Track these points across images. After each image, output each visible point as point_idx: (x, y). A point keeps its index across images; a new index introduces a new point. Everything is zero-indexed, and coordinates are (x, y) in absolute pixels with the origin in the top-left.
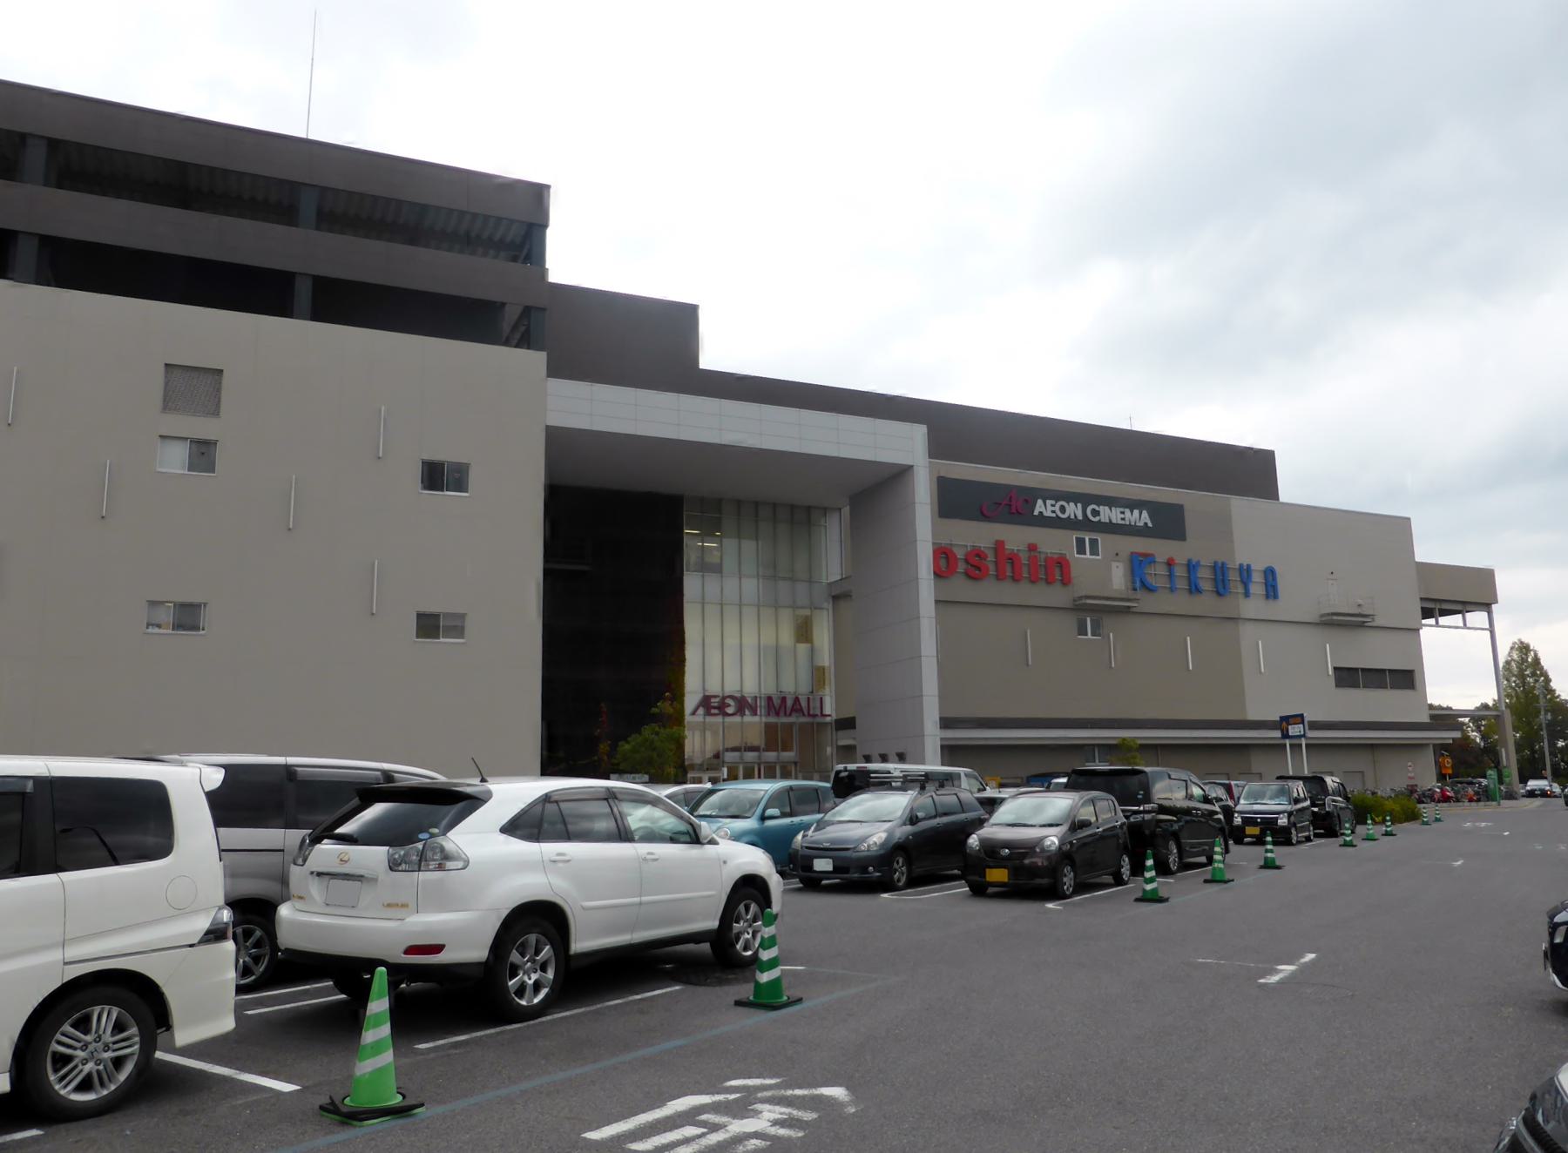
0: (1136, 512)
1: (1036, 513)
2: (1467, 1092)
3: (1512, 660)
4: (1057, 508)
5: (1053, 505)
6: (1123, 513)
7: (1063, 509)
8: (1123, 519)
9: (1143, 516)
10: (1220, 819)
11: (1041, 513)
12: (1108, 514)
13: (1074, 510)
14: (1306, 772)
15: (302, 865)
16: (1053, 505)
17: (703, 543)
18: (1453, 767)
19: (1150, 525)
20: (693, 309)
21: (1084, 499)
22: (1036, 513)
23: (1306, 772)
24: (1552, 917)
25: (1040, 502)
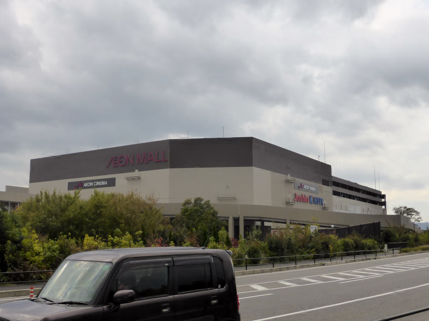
0: (104, 182)
1: (84, 186)
2: (247, 257)
3: (24, 226)
4: (88, 185)
5: (87, 184)
6: (101, 182)
7: (89, 184)
8: (101, 184)
9: (106, 182)
10: (230, 252)
11: (85, 186)
12: (98, 183)
13: (91, 184)
14: (237, 286)
15: (295, 188)
16: (87, 184)
17: (355, 252)
18: (245, 256)
19: (107, 184)
20: (115, 186)
21: (93, 181)
22: (84, 186)
23: (237, 286)
24: (155, 162)
25: (85, 183)
